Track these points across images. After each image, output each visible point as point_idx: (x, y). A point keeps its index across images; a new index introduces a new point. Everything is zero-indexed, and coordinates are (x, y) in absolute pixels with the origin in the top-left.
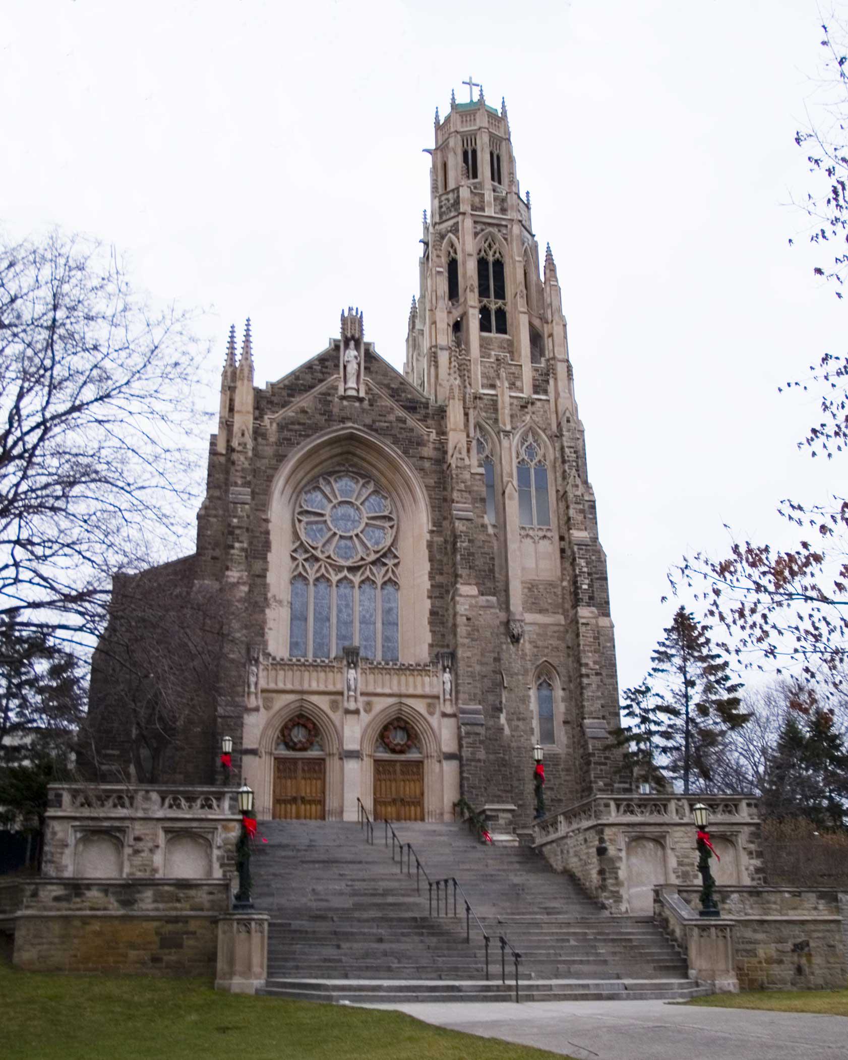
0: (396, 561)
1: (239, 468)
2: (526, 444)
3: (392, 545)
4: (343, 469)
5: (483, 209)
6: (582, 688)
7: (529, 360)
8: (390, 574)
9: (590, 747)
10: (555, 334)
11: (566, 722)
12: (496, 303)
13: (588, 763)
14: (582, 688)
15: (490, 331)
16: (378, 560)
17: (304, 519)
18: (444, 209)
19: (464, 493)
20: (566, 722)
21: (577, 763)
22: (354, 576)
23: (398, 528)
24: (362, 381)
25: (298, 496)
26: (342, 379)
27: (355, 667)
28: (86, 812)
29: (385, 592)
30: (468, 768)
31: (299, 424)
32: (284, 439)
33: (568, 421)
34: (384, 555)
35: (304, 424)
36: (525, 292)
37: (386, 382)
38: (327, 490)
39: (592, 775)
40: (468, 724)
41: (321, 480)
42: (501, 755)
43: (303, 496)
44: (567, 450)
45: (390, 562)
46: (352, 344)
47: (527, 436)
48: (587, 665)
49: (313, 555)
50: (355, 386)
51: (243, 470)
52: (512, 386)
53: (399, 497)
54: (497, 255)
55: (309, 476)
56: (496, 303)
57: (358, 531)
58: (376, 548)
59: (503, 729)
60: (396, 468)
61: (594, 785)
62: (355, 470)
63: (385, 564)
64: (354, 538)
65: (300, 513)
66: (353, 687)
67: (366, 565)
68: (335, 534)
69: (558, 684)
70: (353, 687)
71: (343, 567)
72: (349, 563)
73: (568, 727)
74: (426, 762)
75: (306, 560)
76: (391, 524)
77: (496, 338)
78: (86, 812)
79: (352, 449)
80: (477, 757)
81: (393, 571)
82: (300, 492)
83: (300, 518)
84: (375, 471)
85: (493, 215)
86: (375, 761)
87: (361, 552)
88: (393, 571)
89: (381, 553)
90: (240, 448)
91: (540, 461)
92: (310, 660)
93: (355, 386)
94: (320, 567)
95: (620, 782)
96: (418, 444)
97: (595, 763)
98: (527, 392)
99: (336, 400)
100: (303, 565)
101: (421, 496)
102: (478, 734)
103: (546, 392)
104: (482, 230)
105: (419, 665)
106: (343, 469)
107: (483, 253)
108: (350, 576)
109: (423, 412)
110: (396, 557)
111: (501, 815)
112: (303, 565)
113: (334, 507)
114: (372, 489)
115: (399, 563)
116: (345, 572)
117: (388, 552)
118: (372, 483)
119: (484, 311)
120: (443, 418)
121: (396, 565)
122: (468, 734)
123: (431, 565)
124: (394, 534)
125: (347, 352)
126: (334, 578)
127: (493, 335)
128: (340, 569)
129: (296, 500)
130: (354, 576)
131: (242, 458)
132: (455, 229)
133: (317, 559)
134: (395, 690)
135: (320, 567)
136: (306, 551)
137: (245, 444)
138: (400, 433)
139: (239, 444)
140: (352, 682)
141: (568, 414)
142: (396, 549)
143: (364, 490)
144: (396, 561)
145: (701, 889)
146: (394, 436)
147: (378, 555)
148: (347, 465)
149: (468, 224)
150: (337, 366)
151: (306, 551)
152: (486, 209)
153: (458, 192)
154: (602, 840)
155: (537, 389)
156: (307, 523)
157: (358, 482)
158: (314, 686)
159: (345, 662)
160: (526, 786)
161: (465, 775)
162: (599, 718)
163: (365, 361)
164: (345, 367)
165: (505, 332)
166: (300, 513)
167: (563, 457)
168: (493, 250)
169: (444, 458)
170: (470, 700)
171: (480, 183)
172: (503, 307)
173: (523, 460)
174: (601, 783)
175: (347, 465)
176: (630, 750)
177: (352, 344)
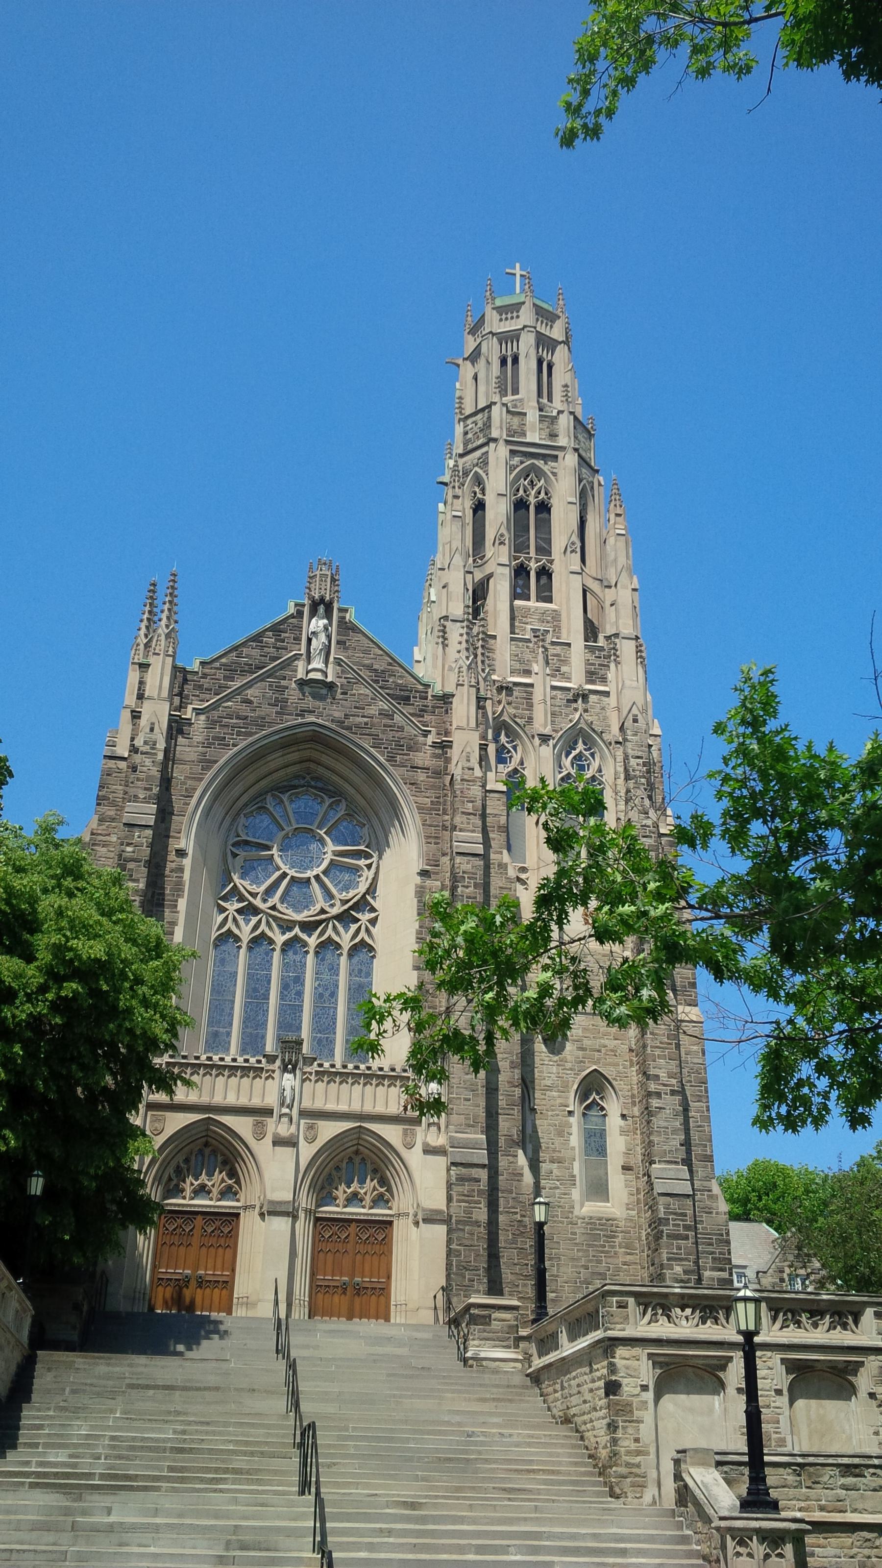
0: (373, 915)
1: (142, 776)
2: (574, 753)
3: (367, 892)
4: (302, 782)
5: (524, 434)
6: (650, 1114)
7: (581, 636)
8: (363, 934)
9: (662, 1209)
10: (619, 601)
11: (626, 1168)
12: (537, 561)
13: (658, 1237)
14: (650, 1114)
15: (528, 599)
17: (242, 853)
18: (470, 436)
19: (472, 817)
20: (626, 1168)
21: (644, 1233)
22: (310, 936)
23: (378, 868)
24: (331, 659)
25: (234, 820)
26: (304, 657)
27: (293, 1071)
29: (355, 960)
30: (461, 1234)
31: (238, 718)
32: (214, 738)
33: (635, 721)
34: (357, 907)
35: (246, 718)
36: (579, 544)
37: (367, 662)
38: (277, 813)
39: (665, 1256)
40: (462, 1164)
41: (269, 798)
42: (518, 1217)
43: (242, 820)
44: (633, 762)
45: (364, 917)
46: (321, 609)
47: (576, 743)
48: (657, 1077)
49: (250, 903)
50: (321, 666)
51: (149, 778)
52: (556, 672)
53: (382, 825)
54: (542, 495)
55: (252, 792)
56: (537, 561)
57: (318, 870)
58: (344, 896)
59: (522, 1175)
60: (378, 783)
61: (667, 1272)
62: (320, 785)
63: (357, 920)
64: (313, 880)
65: (235, 844)
66: (288, 1101)
67: (327, 920)
68: (285, 875)
69: (613, 1107)
70: (288, 1101)
71: (294, 923)
73: (631, 1176)
74: (395, 1223)
75: (238, 911)
76: (368, 862)
77: (537, 608)
79: (315, 755)
80: (474, 1217)
81: (368, 931)
82: (238, 814)
83: (234, 850)
84: (346, 785)
85: (537, 441)
86: (317, 1219)
87: (320, 902)
88: (368, 931)
90: (146, 748)
92: (338, 1065)
93: (321, 666)
94: (260, 921)
95: (713, 1269)
96: (410, 749)
97: (668, 1236)
98: (576, 680)
99: (294, 685)
100: (235, 919)
101: (411, 818)
102: (478, 1180)
103: (604, 680)
104: (522, 463)
105: (393, 1070)
106: (302, 782)
107: (521, 492)
108: (304, 936)
109: (419, 703)
110: (373, 910)
111: (496, 1315)
112: (235, 919)
113: (286, 836)
114: (343, 813)
115: (376, 918)
116: (297, 930)
117: (362, 904)
118: (343, 805)
119: (521, 572)
120: (447, 712)
121: (373, 922)
122: (461, 1179)
123: (421, 921)
125: (314, 620)
126: (280, 939)
127: (532, 604)
128: (286, 926)
129: (231, 824)
130: (310, 936)
131: (148, 762)
132: (484, 462)
133: (256, 911)
134: (356, 1107)
135: (260, 921)
136: (242, 899)
137: (155, 743)
138: (384, 732)
139: (146, 743)
140: (288, 1093)
141: (635, 711)
142: (374, 898)
143: (332, 812)
144: (373, 915)
145: (746, 1459)
146: (375, 736)
147: (346, 907)
148: (308, 778)
149: (499, 454)
150: (298, 639)
151: (242, 899)
152: (528, 434)
153: (490, 412)
154: (612, 1368)
155: (592, 676)
157: (323, 801)
158: (231, 1100)
159: (278, 1062)
160: (562, 1269)
161: (453, 1246)
162: (676, 1163)
163: (338, 634)
164: (309, 641)
165: (549, 600)
166: (235, 844)
167: (626, 770)
168: (536, 488)
169: (446, 768)
170: (469, 1126)
171: (521, 400)
173: (569, 776)
174: (678, 1269)
175: (308, 778)
176: (106, 1194)
177: (321, 609)
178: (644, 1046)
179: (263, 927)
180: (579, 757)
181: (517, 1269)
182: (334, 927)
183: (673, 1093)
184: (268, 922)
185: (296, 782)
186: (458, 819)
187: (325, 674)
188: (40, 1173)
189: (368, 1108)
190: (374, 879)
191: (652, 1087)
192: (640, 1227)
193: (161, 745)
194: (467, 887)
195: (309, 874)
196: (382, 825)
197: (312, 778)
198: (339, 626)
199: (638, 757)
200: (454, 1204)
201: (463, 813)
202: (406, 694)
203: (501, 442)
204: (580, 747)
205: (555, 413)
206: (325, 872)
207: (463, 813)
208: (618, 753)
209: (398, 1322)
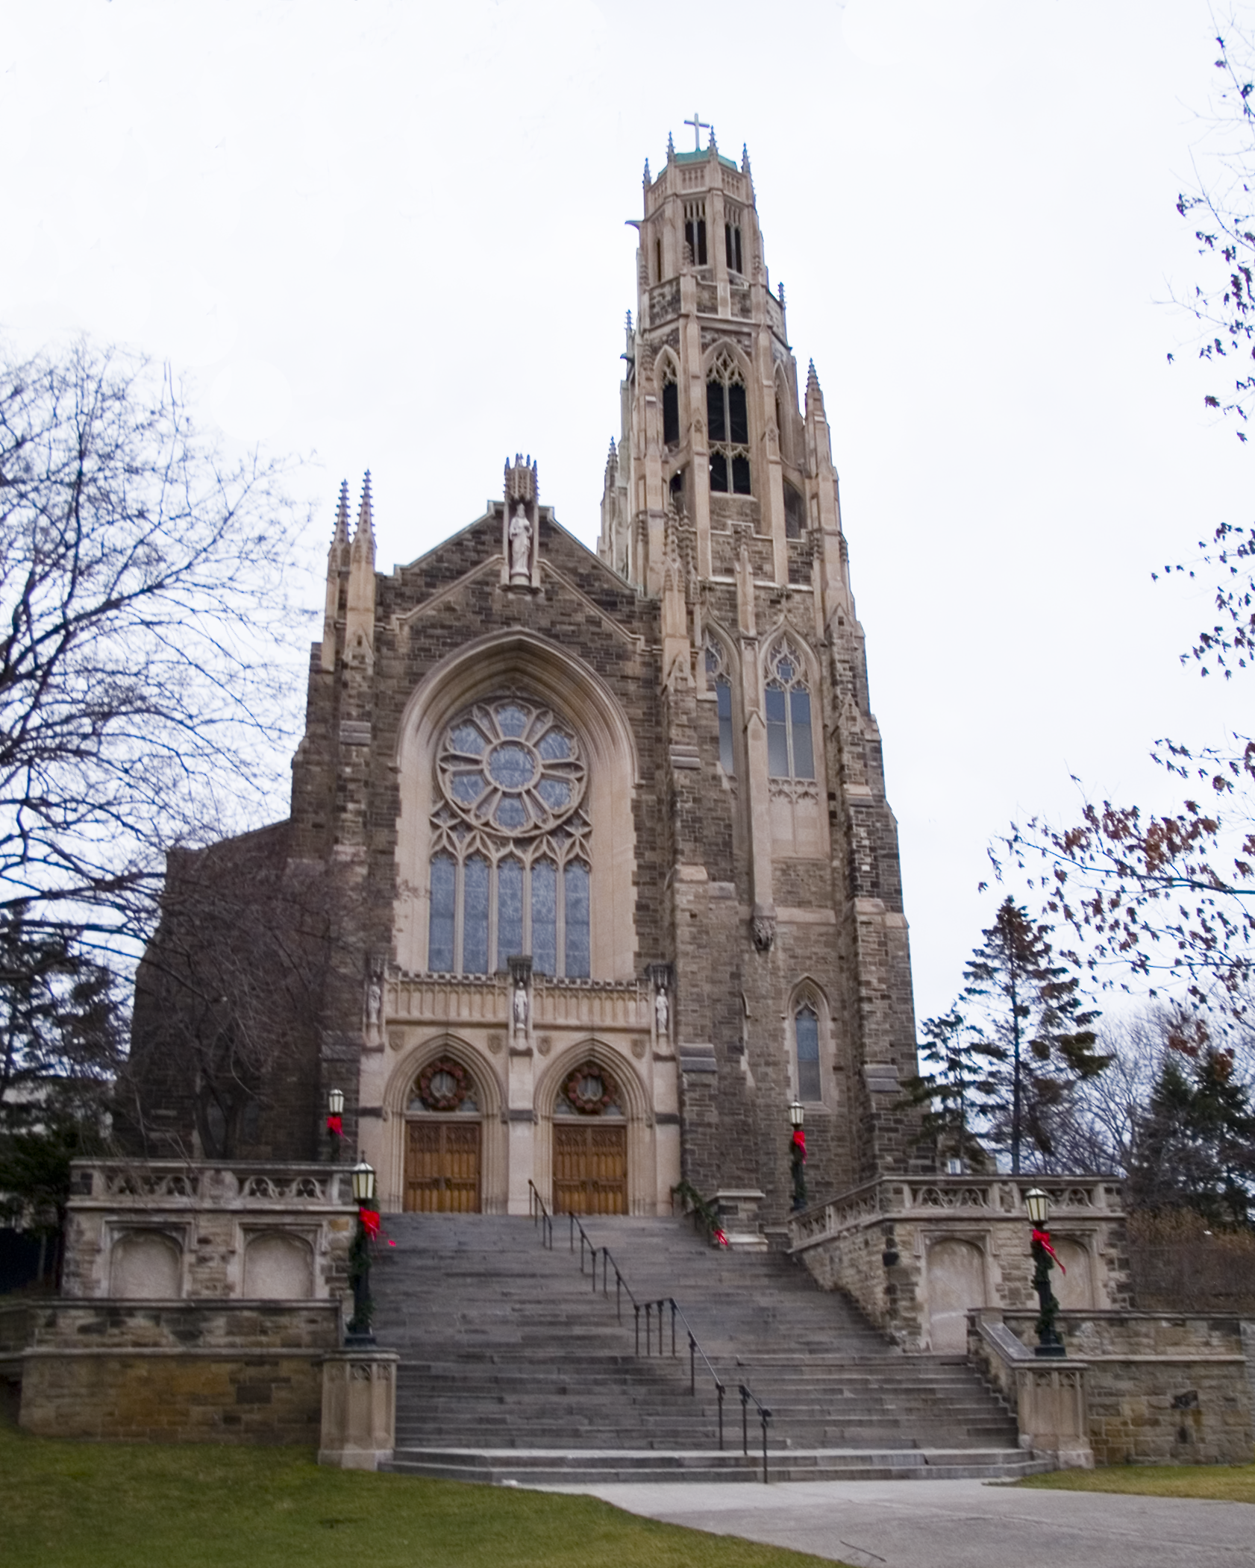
0: (586, 830)
1: (353, 692)
2: (779, 657)
3: (580, 806)
4: (508, 693)
5: (714, 310)
6: (862, 1018)
7: (783, 532)
8: (577, 849)
9: (874, 1104)
11: (837, 1069)
13: (871, 1129)
14: (862, 1018)
15: (725, 490)
16: (560, 828)
17: (451, 767)
18: (657, 309)
19: (686, 730)
20: (837, 1069)
21: (854, 1128)
22: (525, 851)
24: (535, 563)
25: (441, 734)
27: (526, 987)
28: (127, 1201)
29: (570, 875)
30: (693, 1136)
31: (443, 627)
32: (421, 649)
33: (841, 623)
34: (569, 822)
35: (450, 627)
36: (777, 431)
37: (571, 565)
38: (484, 725)
39: (877, 1147)
41: (475, 711)
44: (839, 666)
45: (577, 831)
46: (521, 508)
47: (780, 644)
48: (868, 983)
50: (525, 571)
51: (360, 695)
52: (758, 571)
53: (593, 740)
54: (736, 377)
55: (458, 704)
57: (530, 785)
58: (556, 811)
59: (744, 1079)
62: (525, 695)
63: (570, 835)
64: (525, 796)
65: (445, 759)
66: (522, 1016)
67: (542, 835)
68: (496, 790)
69: (825, 1012)
70: (522, 1016)
72: (516, 833)
74: (630, 1127)
75: (453, 828)
76: (579, 775)
77: (734, 500)
78: (127, 1201)
79: (521, 664)
81: (581, 845)
82: (444, 728)
83: (444, 766)
87: (534, 817)
88: (581, 845)
89: (564, 818)
90: (355, 663)
91: (799, 682)
93: (525, 571)
94: (474, 838)
95: (918, 1157)
96: (619, 657)
97: (880, 1129)
98: (780, 580)
100: (448, 836)
101: (623, 733)
102: (708, 1086)
103: (807, 580)
105: (621, 984)
106: (508, 693)
107: (714, 374)
108: (518, 852)
109: (626, 609)
110: (586, 824)
113: (495, 749)
114: (550, 724)
115: (590, 832)
116: (511, 847)
117: (575, 817)
119: (717, 460)
121: (586, 836)
122: (693, 1085)
124: (583, 790)
125: (514, 520)
126: (495, 856)
127: (730, 495)
128: (503, 841)
129: (439, 739)
130: (525, 851)
132: (673, 339)
133: (469, 828)
134: (585, 1020)
135: (474, 838)
136: (454, 815)
137: (363, 657)
138: (592, 641)
139: (354, 657)
140: (521, 1010)
141: (840, 613)
142: (586, 812)
143: (539, 725)
144: (586, 830)
146: (583, 645)
147: (559, 822)
150: (499, 541)
151: (454, 815)
152: (720, 309)
153: (678, 284)
154: (890, 1243)
155: (794, 575)
156: (455, 774)
157: (529, 712)
158: (465, 1015)
159: (510, 980)
162: (886, 1063)
163: (541, 535)
164: (510, 543)
166: (445, 759)
167: (833, 675)
168: (729, 370)
169: (657, 677)
170: (696, 1035)
171: (710, 271)
172: (744, 454)
173: (774, 680)
174: (889, 1159)
175: (513, 688)
177: (521, 508)
178: (856, 954)
179: (478, 843)
180: (784, 661)
181: (743, 1165)
182: (548, 841)
183: (883, 997)
184: (482, 838)
185: (499, 693)
186: (674, 732)
187: (529, 578)
188: (1040, 1192)
189: (597, 1022)
190: (586, 793)
191: (864, 992)
192: (851, 1122)
193: (370, 658)
194: (686, 802)
195: (521, 789)
196: (593, 740)
197: (518, 689)
198: (540, 527)
199: (844, 661)
200: (687, 1108)
201: (678, 725)
202: (612, 599)
203: (692, 318)
204: (785, 649)
205: (746, 287)
206: (535, 787)
207: (678, 725)
208: (824, 658)
209: (464, 1193)
